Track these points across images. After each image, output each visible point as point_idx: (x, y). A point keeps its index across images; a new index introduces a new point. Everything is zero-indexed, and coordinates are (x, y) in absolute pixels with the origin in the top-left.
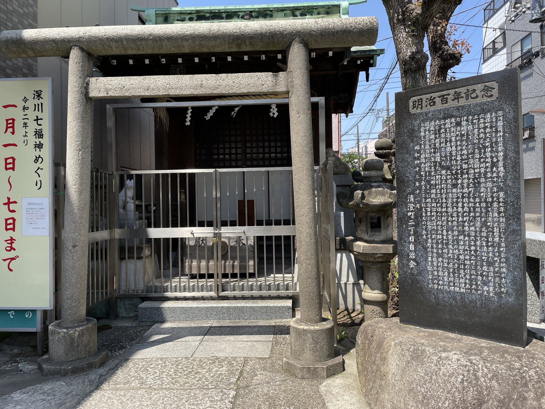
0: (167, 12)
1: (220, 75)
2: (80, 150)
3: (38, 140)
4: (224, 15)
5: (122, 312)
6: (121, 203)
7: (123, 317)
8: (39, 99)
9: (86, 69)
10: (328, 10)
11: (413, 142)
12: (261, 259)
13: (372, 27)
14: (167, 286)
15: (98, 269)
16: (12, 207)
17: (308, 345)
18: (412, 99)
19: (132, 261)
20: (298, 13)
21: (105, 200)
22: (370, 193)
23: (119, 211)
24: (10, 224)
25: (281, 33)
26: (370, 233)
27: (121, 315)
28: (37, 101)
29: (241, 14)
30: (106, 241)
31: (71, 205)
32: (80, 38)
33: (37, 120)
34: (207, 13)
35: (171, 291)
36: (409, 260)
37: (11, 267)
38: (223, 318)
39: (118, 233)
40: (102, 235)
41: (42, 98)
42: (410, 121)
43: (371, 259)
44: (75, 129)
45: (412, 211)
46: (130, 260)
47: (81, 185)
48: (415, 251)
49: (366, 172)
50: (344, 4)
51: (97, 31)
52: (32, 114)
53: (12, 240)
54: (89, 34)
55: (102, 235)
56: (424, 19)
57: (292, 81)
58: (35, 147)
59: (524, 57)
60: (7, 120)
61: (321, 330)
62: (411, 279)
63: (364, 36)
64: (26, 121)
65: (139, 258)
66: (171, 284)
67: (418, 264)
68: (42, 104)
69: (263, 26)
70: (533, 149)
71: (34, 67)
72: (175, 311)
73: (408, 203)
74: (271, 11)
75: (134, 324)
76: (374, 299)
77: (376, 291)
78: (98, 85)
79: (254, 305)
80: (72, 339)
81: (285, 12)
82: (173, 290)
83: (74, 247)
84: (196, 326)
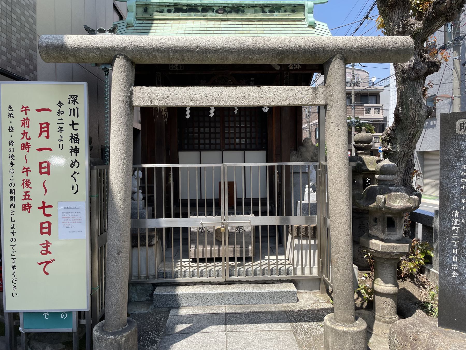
0: (147, 3)
1: (262, 87)
2: (125, 159)
3: (74, 145)
4: (200, 9)
7: (135, 301)
8: (74, 104)
9: (130, 78)
10: (294, 8)
11: (459, 161)
13: (408, 47)
14: (177, 272)
16: (47, 211)
17: (347, 345)
18: (459, 121)
19: (143, 248)
20: (267, 10)
22: (390, 197)
24: (46, 228)
25: (323, 50)
26: (386, 233)
28: (72, 106)
29: (216, 9)
31: (116, 212)
32: (125, 47)
33: (73, 124)
34: (184, 6)
35: (181, 277)
36: (451, 270)
37: (46, 270)
38: (235, 304)
41: (77, 103)
42: (457, 141)
43: (387, 257)
45: (456, 226)
47: (125, 192)
48: (458, 262)
49: (382, 176)
50: (309, 4)
51: (143, 41)
52: (67, 119)
53: (47, 244)
54: (135, 44)
56: (425, 34)
57: (332, 95)
58: (71, 151)
60: (41, 124)
61: (359, 331)
62: (452, 287)
63: (400, 55)
64: (61, 125)
65: (150, 245)
67: (461, 274)
68: (77, 109)
69: (307, 41)
70: (434, 126)
71: (34, 57)
73: (452, 218)
74: (243, 7)
76: (388, 292)
77: (389, 285)
78: (142, 95)
79: (262, 290)
80: (120, 345)
81: (255, 8)
83: (119, 254)
84: (211, 312)
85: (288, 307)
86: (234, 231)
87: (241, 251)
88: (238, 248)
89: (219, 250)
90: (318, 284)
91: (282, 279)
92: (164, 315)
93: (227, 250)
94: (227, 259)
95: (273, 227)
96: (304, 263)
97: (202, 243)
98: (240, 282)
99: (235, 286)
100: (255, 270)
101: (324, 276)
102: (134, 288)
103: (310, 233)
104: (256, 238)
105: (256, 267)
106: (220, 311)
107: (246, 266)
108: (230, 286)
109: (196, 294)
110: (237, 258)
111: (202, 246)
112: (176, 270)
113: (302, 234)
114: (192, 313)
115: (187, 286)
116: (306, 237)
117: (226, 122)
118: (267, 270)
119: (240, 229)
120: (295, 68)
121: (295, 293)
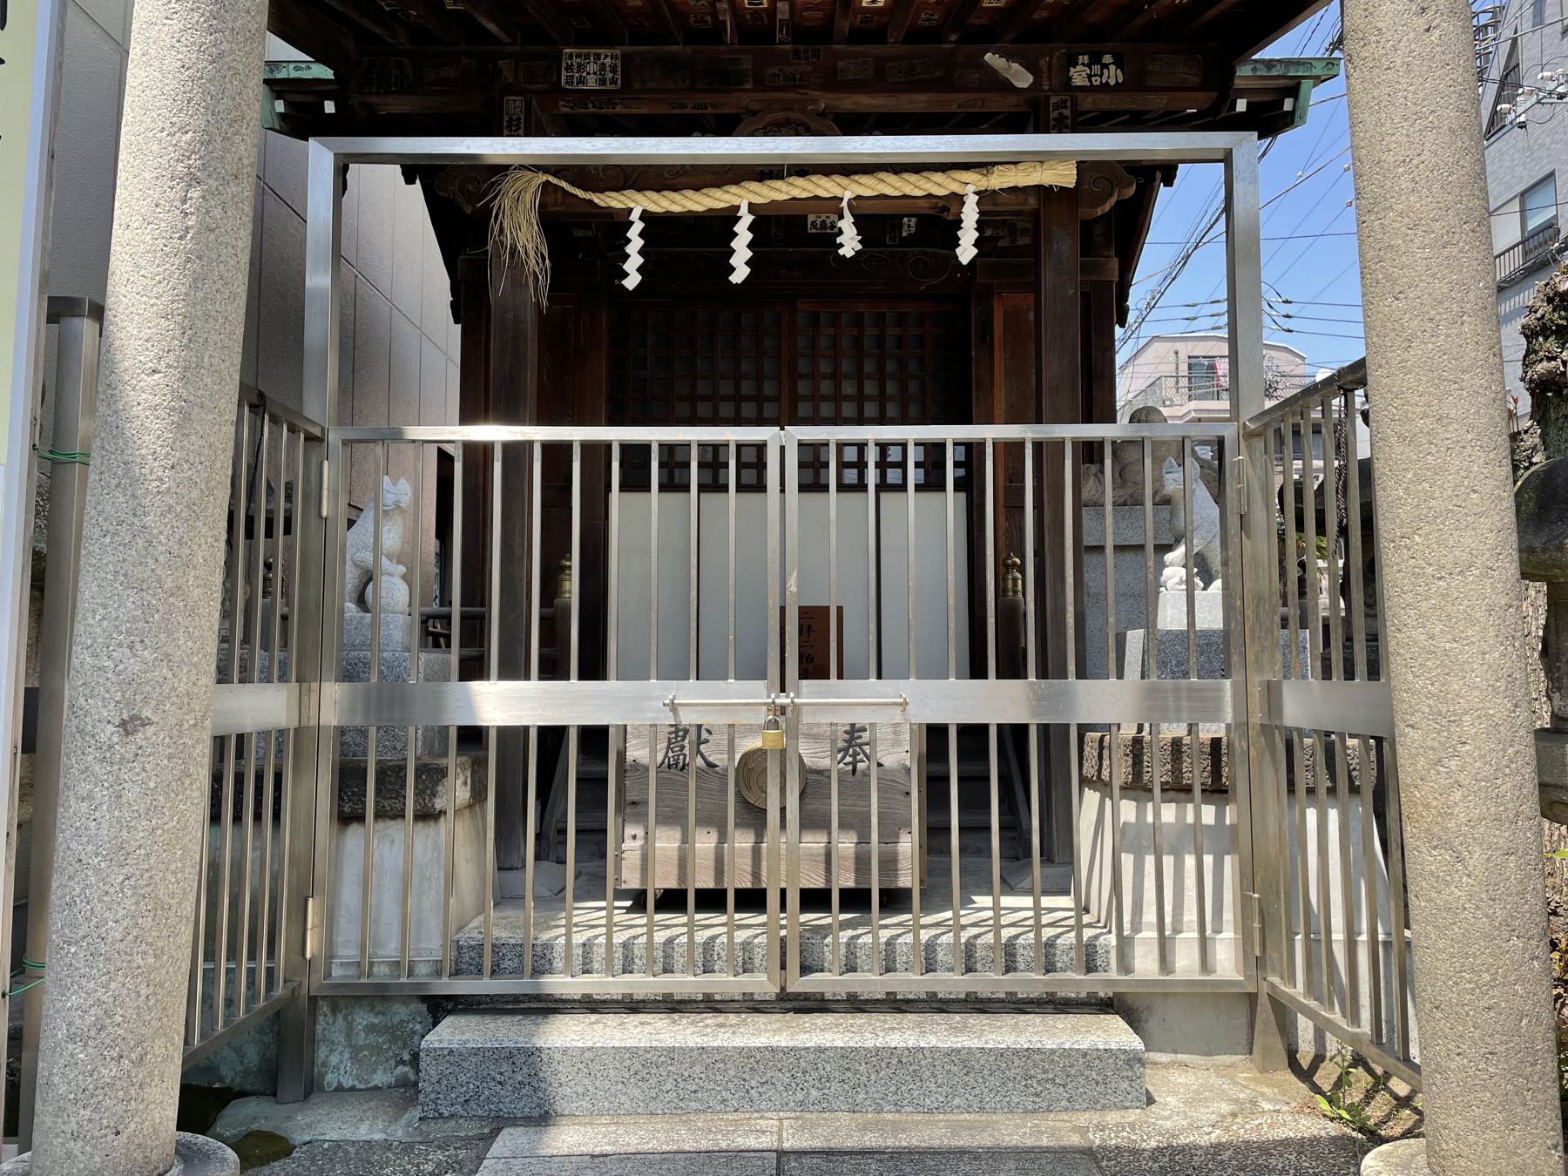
2: (192, 180)
5: (337, 1062)
6: (351, 578)
7: (340, 1089)
12: (935, 834)
15: (238, 867)
19: (394, 828)
21: (265, 594)
23: (342, 611)
27: (331, 1079)
30: (282, 733)
35: (568, 970)
39: (333, 703)
40: (263, 706)
44: (172, 62)
46: (381, 825)
47: (188, 372)
55: (263, 706)
59: (1531, 244)
65: (427, 815)
66: (568, 935)
72: (595, 1067)
75: (399, 1132)
82: (577, 962)
83: (128, 726)
84: (704, 1145)
85: (1101, 1128)
86: (825, 763)
87: (862, 863)
88: (846, 844)
89: (756, 854)
90: (1243, 1021)
91: (1062, 993)
92: (462, 1154)
93: (797, 855)
94: (793, 900)
95: (1015, 735)
96: (1168, 919)
97: (673, 816)
98: (856, 1004)
99: (829, 1018)
100: (930, 947)
101: (1276, 980)
102: (340, 1019)
103: (1196, 772)
104: (935, 786)
105: (933, 932)
106: (752, 1142)
107: (886, 927)
108: (806, 1018)
109: (633, 1052)
110: (842, 891)
111: (676, 833)
112: (545, 936)
113: (1158, 773)
114: (608, 1149)
115: (594, 1017)
116: (1178, 789)
117: (801, 376)
118: (990, 947)
119: (855, 755)
120: (1096, 81)
121: (1134, 1060)
